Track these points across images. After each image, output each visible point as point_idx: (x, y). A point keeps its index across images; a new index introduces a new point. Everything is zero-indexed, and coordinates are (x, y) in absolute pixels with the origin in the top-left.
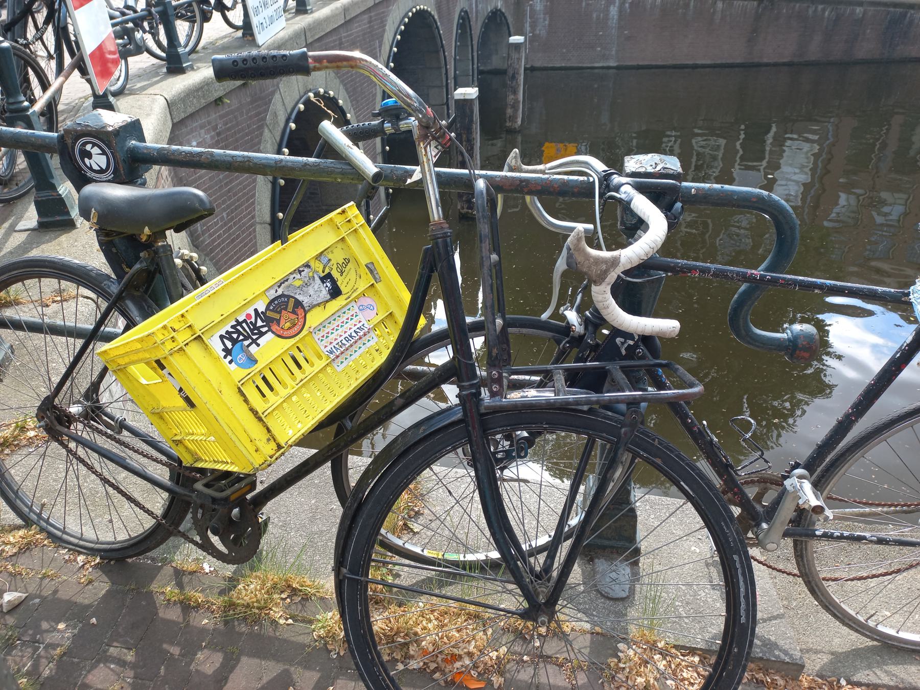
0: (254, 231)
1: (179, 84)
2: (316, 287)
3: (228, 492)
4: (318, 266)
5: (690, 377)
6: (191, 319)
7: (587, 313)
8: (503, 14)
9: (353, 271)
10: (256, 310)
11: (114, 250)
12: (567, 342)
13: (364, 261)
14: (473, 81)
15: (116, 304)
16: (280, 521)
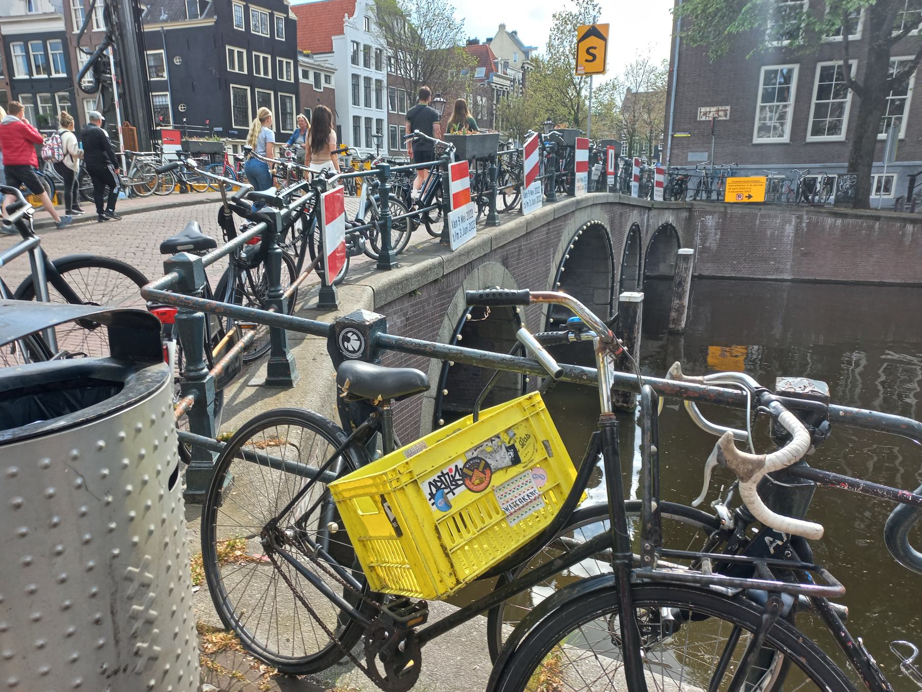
0: (421, 403)
1: (385, 278)
2: (502, 454)
3: (407, 618)
4: (505, 438)
5: (832, 579)
6: (412, 467)
7: (738, 510)
8: (674, 228)
9: (532, 445)
10: (456, 466)
11: (347, 409)
12: (717, 534)
13: (541, 438)
14: (638, 285)
15: (342, 450)
16: (428, 670)
